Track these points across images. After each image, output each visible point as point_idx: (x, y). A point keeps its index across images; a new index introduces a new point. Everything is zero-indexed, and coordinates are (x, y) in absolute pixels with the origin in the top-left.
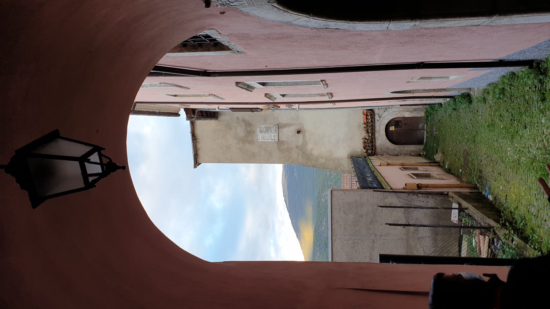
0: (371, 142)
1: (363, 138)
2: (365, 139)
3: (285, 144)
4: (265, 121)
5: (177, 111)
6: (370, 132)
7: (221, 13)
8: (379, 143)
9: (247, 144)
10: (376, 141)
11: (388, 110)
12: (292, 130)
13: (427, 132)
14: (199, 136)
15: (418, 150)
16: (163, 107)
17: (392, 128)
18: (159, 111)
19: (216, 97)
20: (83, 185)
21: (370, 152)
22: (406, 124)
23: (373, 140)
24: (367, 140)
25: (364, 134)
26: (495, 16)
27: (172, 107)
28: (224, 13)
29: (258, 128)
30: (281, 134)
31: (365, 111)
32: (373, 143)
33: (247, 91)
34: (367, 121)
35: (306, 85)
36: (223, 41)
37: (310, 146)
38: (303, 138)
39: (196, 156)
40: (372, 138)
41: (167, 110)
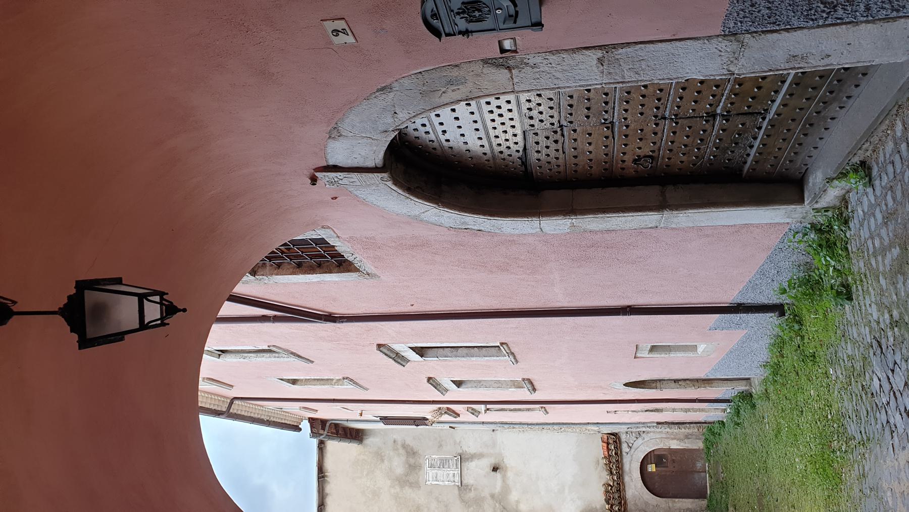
0: (617, 491)
1: (604, 484)
2: (607, 486)
3: (473, 489)
4: (439, 447)
5: (297, 422)
6: (615, 472)
7: (332, 199)
8: (631, 494)
9: (407, 488)
10: (627, 489)
11: (643, 435)
12: (485, 464)
13: (710, 476)
14: (328, 471)
15: (698, 509)
16: (276, 412)
17: (652, 468)
18: (268, 419)
19: (354, 383)
20: (137, 326)
21: (617, 508)
22: (674, 461)
23: (621, 487)
24: (610, 488)
25: (605, 477)
26: (665, 211)
27: (289, 415)
28: (336, 198)
29: (427, 460)
30: (465, 472)
31: (605, 437)
32: (620, 493)
33: (396, 364)
34: (608, 453)
35: (485, 357)
36: (345, 252)
37: (514, 496)
38: (503, 480)
39: (322, 507)
40: (619, 484)
41: (282, 419)
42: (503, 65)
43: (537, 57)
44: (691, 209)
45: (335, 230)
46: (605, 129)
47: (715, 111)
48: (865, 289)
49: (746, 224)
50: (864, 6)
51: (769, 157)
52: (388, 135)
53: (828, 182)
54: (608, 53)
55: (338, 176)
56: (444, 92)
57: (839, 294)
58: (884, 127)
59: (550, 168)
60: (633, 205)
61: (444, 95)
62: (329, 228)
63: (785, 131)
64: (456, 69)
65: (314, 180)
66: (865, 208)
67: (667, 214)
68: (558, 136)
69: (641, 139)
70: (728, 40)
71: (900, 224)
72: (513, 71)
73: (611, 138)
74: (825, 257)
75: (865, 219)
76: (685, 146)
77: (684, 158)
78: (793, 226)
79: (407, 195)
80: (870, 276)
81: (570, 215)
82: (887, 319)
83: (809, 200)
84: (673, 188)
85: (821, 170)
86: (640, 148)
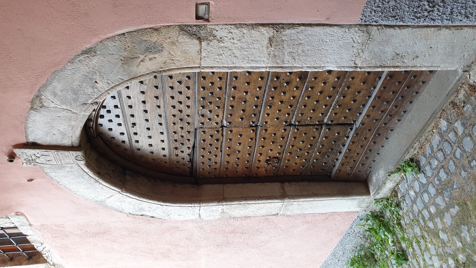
7: (29, 181)
28: (32, 180)
36: (35, 241)
42: (195, 35)
43: (224, 29)
44: (302, 198)
45: (28, 217)
46: (252, 131)
47: (323, 121)
48: (423, 247)
49: (333, 212)
50: (451, 9)
51: (350, 161)
52: (87, 108)
53: (389, 175)
54: (278, 32)
55: (36, 153)
56: (142, 61)
57: (398, 257)
58: (430, 128)
59: (210, 165)
60: (265, 195)
61: (141, 63)
62: (22, 214)
63: (363, 139)
64: (155, 33)
65: (12, 157)
66: (416, 189)
67: (287, 201)
68: (219, 136)
69: (273, 142)
70: (361, 31)
71: (456, 189)
72: (203, 43)
73: (254, 140)
74: (384, 233)
75: (417, 197)
76: (300, 149)
77: (298, 161)
78: (360, 214)
79: (97, 178)
80: (429, 236)
81: (223, 201)
82: (452, 264)
83: (374, 192)
84: (289, 184)
85: (382, 169)
86: (271, 150)
